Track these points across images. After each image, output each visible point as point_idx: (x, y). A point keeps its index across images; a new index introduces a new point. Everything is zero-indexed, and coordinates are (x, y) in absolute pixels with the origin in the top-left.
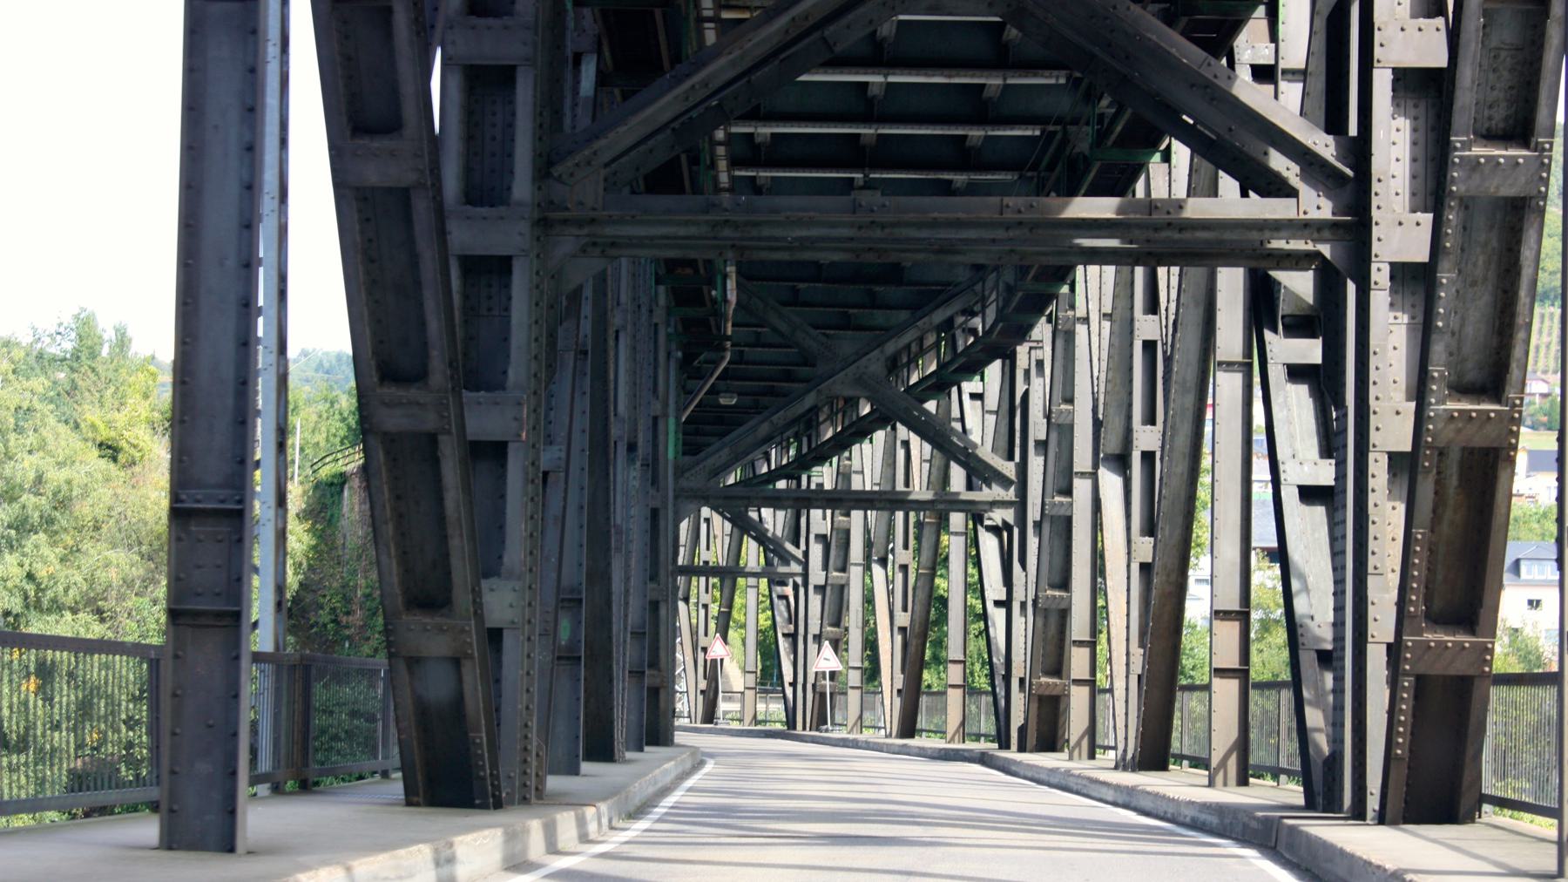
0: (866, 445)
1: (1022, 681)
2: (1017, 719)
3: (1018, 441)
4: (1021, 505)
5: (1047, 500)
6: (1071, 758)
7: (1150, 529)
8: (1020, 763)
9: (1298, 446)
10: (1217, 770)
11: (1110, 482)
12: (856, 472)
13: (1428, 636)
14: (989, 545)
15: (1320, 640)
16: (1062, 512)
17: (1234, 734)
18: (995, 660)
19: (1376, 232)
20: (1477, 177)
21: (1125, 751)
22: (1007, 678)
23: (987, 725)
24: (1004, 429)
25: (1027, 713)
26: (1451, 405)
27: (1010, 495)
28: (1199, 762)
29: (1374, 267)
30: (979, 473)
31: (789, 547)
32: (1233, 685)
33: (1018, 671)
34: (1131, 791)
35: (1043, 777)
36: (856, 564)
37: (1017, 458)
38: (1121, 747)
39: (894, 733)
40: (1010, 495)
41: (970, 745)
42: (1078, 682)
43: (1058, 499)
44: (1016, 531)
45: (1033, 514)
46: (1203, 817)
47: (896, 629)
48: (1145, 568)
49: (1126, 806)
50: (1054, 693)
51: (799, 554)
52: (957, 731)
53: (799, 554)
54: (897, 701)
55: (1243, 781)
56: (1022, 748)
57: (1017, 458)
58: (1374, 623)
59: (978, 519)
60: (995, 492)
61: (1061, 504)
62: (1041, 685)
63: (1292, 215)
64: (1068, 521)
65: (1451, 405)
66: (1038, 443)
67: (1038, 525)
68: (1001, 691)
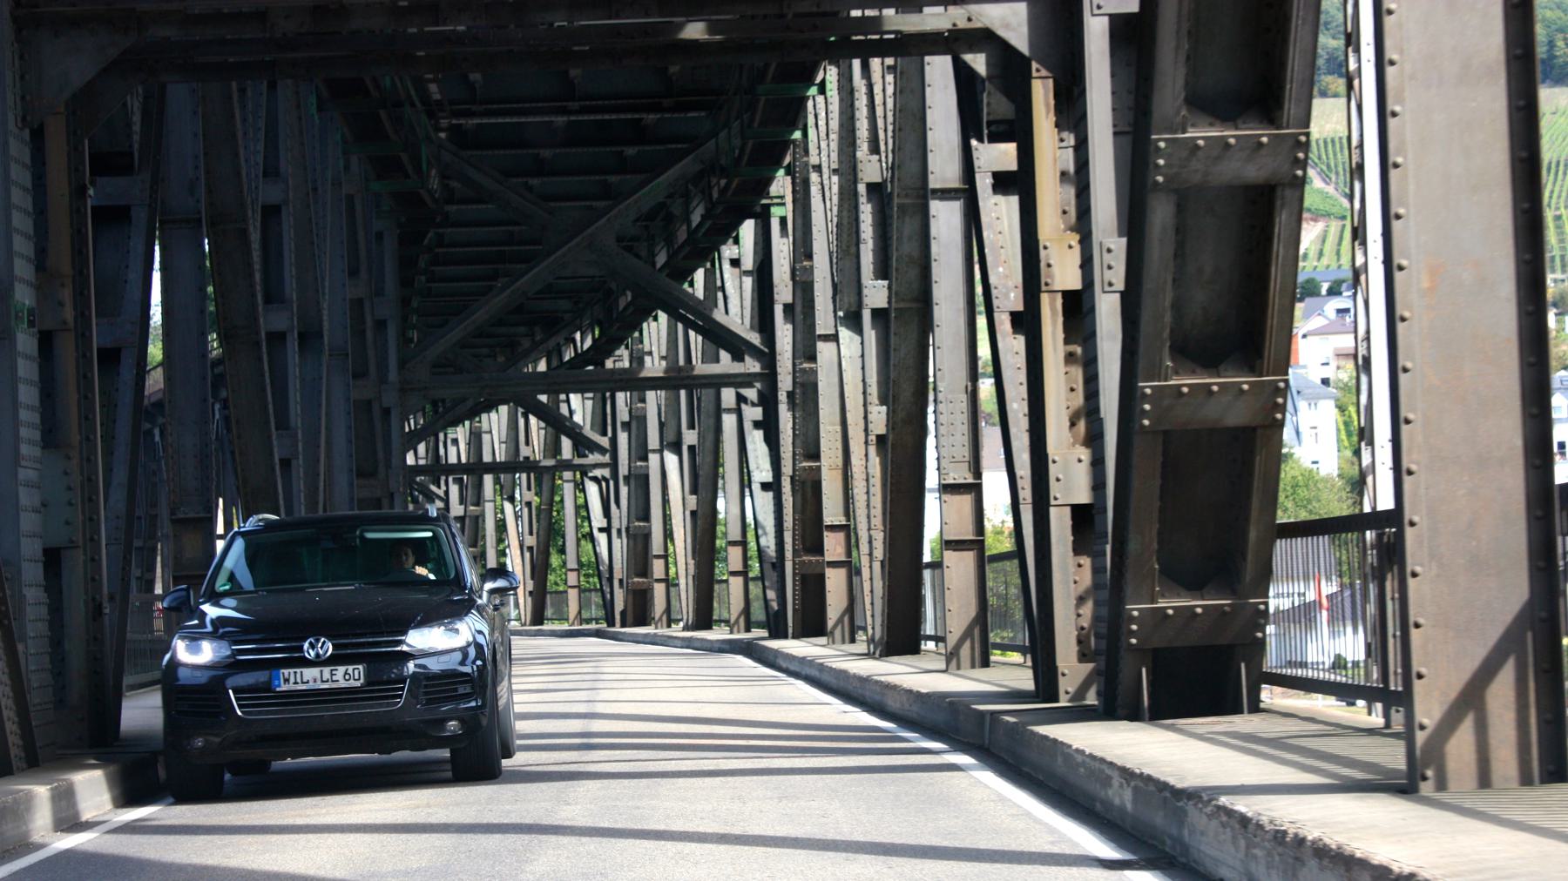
0: (493, 415)
1: (621, 581)
2: (619, 606)
3: (609, 421)
4: (614, 465)
5: (632, 465)
6: (656, 628)
7: (694, 491)
8: (624, 633)
9: (760, 462)
10: (734, 625)
11: (671, 459)
12: (486, 432)
13: (805, 558)
14: (592, 490)
15: (771, 557)
16: (642, 472)
17: (742, 605)
18: (601, 568)
19: (779, 378)
20: (805, 377)
21: (688, 620)
22: (611, 579)
23: (595, 611)
24: (599, 411)
25: (626, 602)
26: (805, 464)
27: (607, 458)
28: (727, 622)
29: (780, 393)
30: (583, 445)
31: (433, 488)
32: (969, 557)
33: (617, 575)
34: (690, 639)
35: (640, 639)
36: (489, 501)
37: (610, 434)
38: (685, 618)
39: (528, 622)
40: (607, 458)
41: (585, 627)
42: (658, 581)
43: (639, 464)
44: (612, 483)
45: (623, 470)
46: (724, 646)
47: (525, 549)
48: (693, 513)
49: (687, 647)
50: (643, 588)
51: (441, 493)
52: (576, 617)
53: (441, 493)
54: (529, 600)
55: (748, 630)
56: (623, 625)
57: (610, 434)
58: (1057, 484)
59: (584, 474)
60: (594, 458)
61: (641, 466)
62: (634, 583)
63: (742, 371)
64: (647, 477)
65: (805, 464)
66: (623, 424)
67: (627, 479)
68: (607, 590)
